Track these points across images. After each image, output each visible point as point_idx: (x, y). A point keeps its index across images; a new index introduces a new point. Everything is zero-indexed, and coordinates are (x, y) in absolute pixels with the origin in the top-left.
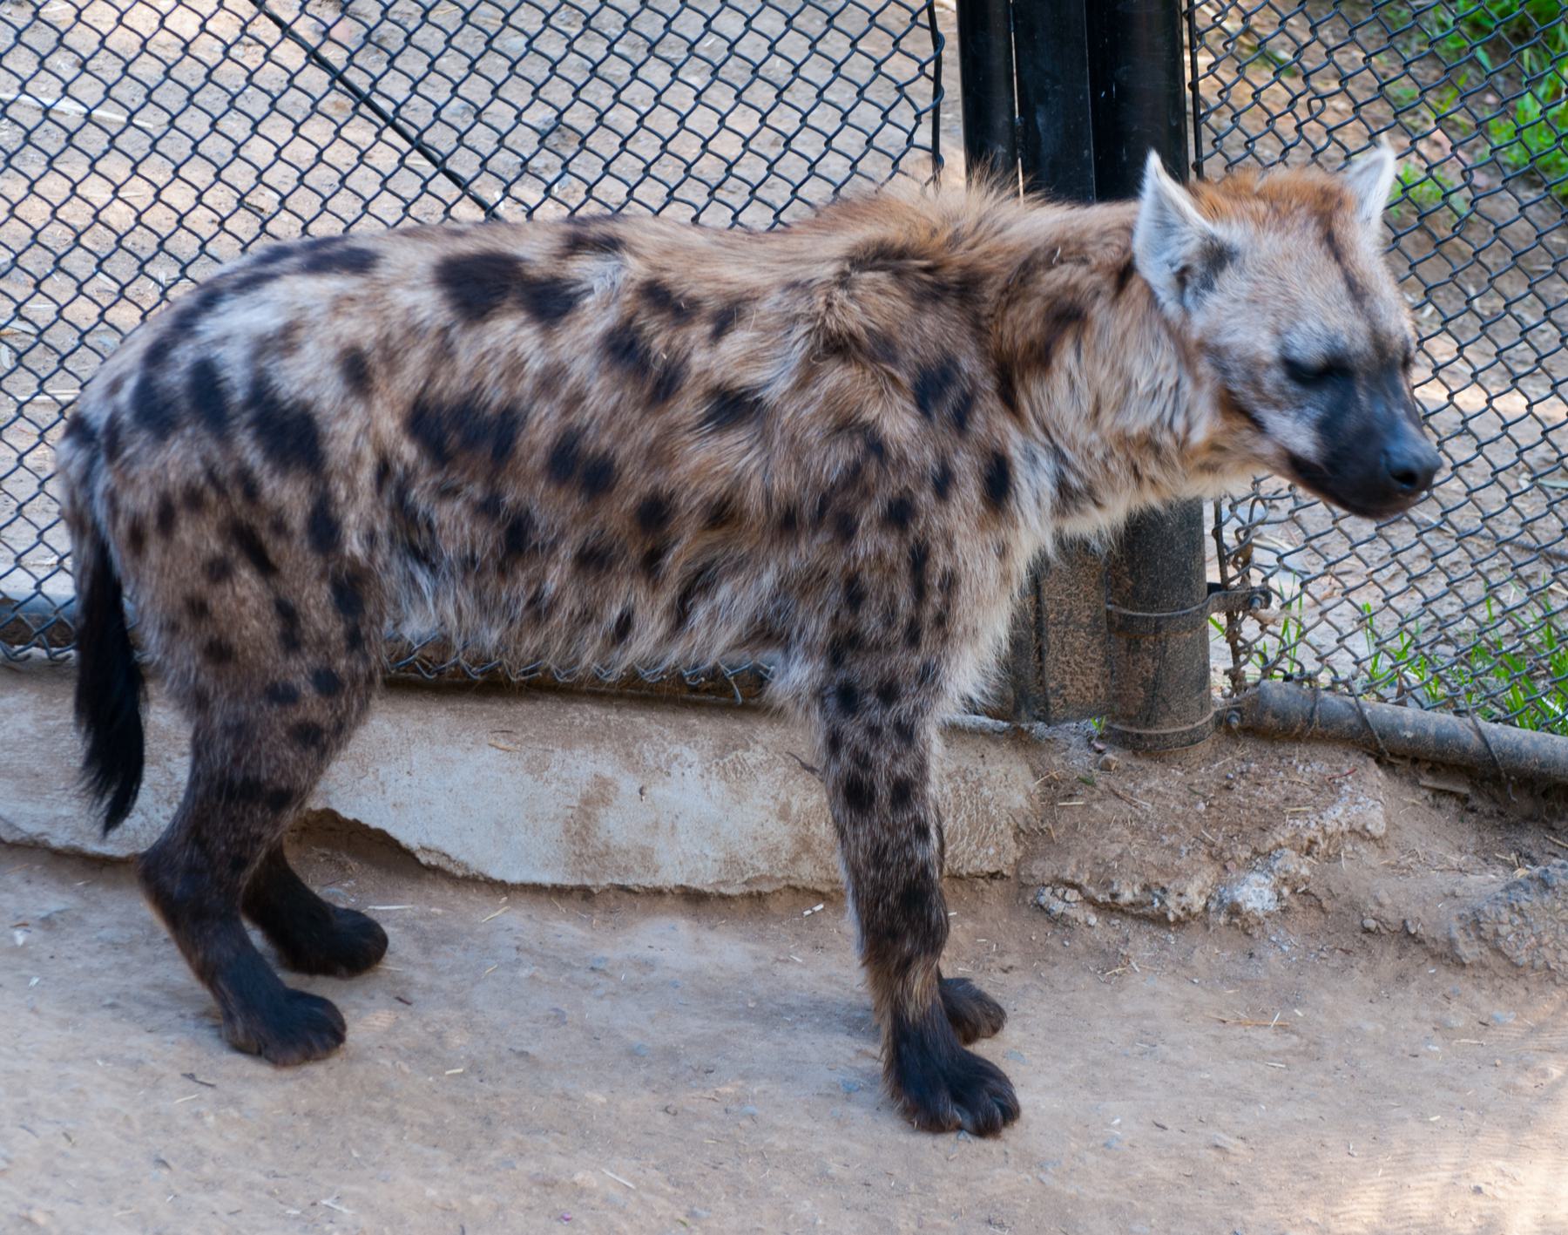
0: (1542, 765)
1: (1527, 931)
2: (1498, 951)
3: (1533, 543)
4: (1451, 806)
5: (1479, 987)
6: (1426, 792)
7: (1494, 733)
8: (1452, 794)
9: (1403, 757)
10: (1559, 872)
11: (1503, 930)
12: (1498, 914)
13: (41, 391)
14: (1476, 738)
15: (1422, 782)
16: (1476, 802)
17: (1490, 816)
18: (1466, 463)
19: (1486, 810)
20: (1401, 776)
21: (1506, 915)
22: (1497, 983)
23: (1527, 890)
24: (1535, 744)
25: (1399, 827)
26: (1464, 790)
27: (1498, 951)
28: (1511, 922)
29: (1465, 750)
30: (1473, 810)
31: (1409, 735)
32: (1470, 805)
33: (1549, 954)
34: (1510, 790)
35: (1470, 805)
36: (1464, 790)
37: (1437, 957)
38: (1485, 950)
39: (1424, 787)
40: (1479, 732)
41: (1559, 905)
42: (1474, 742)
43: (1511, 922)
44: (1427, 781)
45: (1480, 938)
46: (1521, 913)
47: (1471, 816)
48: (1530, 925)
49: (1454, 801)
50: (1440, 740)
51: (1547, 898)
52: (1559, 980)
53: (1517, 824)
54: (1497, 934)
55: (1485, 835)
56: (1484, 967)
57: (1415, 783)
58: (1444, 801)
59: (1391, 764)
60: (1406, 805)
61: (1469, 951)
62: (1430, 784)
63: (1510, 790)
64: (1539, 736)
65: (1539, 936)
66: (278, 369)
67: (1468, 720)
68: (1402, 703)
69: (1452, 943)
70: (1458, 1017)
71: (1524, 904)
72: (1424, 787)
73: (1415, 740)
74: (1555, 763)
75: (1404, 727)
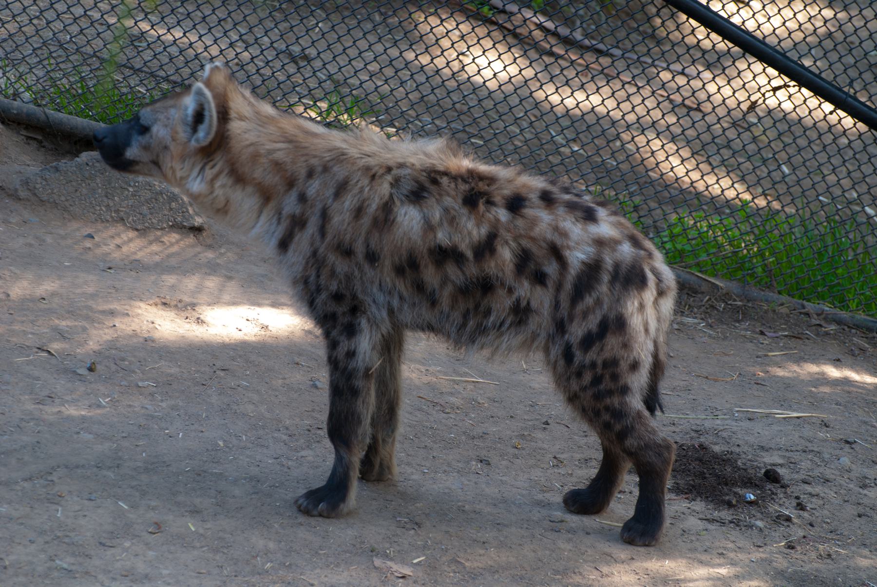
0: (71, 129)
1: (47, 187)
2: (35, 194)
3: (738, 128)
4: (34, 144)
5: (25, 208)
6: (23, 137)
7: (51, 114)
8: (35, 139)
9: (14, 122)
10: (64, 165)
11: (38, 186)
12: (36, 180)
13: (214, 13)
14: (44, 115)
15: (21, 133)
16: (45, 144)
17: (51, 150)
18: (224, 19)
19: (50, 147)
20: (12, 130)
21: (39, 180)
22: (33, 207)
23: (49, 171)
24: (68, 119)
25: (7, 148)
26: (40, 138)
27: (35, 194)
28: (41, 183)
29: (39, 120)
30: (44, 147)
31: (15, 112)
32: (43, 144)
33: (56, 197)
34: (59, 139)
35: (43, 144)
36: (40, 138)
37: (10, 196)
38: (30, 194)
39: (22, 135)
40: (45, 113)
41: (62, 178)
42: (43, 117)
43: (41, 183)
44: (24, 132)
45: (28, 189)
46: (46, 180)
47: (43, 149)
48: (48, 185)
49: (36, 142)
50: (28, 115)
51: (57, 175)
52: (59, 208)
53: (62, 154)
54: (35, 188)
55: (48, 156)
56: (29, 200)
57: (18, 133)
58: (31, 142)
59: (8, 125)
60: (13, 141)
61: (22, 194)
62: (25, 134)
63: (59, 139)
64: (70, 117)
65: (52, 189)
66: (364, 360)
67: (41, 109)
68: (15, 100)
69: (16, 190)
70: (14, 219)
71: (48, 177)
72: (22, 135)
73: (18, 114)
74: (77, 128)
75: (13, 109)
